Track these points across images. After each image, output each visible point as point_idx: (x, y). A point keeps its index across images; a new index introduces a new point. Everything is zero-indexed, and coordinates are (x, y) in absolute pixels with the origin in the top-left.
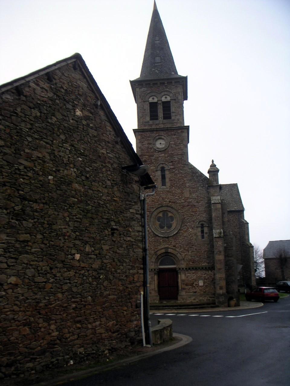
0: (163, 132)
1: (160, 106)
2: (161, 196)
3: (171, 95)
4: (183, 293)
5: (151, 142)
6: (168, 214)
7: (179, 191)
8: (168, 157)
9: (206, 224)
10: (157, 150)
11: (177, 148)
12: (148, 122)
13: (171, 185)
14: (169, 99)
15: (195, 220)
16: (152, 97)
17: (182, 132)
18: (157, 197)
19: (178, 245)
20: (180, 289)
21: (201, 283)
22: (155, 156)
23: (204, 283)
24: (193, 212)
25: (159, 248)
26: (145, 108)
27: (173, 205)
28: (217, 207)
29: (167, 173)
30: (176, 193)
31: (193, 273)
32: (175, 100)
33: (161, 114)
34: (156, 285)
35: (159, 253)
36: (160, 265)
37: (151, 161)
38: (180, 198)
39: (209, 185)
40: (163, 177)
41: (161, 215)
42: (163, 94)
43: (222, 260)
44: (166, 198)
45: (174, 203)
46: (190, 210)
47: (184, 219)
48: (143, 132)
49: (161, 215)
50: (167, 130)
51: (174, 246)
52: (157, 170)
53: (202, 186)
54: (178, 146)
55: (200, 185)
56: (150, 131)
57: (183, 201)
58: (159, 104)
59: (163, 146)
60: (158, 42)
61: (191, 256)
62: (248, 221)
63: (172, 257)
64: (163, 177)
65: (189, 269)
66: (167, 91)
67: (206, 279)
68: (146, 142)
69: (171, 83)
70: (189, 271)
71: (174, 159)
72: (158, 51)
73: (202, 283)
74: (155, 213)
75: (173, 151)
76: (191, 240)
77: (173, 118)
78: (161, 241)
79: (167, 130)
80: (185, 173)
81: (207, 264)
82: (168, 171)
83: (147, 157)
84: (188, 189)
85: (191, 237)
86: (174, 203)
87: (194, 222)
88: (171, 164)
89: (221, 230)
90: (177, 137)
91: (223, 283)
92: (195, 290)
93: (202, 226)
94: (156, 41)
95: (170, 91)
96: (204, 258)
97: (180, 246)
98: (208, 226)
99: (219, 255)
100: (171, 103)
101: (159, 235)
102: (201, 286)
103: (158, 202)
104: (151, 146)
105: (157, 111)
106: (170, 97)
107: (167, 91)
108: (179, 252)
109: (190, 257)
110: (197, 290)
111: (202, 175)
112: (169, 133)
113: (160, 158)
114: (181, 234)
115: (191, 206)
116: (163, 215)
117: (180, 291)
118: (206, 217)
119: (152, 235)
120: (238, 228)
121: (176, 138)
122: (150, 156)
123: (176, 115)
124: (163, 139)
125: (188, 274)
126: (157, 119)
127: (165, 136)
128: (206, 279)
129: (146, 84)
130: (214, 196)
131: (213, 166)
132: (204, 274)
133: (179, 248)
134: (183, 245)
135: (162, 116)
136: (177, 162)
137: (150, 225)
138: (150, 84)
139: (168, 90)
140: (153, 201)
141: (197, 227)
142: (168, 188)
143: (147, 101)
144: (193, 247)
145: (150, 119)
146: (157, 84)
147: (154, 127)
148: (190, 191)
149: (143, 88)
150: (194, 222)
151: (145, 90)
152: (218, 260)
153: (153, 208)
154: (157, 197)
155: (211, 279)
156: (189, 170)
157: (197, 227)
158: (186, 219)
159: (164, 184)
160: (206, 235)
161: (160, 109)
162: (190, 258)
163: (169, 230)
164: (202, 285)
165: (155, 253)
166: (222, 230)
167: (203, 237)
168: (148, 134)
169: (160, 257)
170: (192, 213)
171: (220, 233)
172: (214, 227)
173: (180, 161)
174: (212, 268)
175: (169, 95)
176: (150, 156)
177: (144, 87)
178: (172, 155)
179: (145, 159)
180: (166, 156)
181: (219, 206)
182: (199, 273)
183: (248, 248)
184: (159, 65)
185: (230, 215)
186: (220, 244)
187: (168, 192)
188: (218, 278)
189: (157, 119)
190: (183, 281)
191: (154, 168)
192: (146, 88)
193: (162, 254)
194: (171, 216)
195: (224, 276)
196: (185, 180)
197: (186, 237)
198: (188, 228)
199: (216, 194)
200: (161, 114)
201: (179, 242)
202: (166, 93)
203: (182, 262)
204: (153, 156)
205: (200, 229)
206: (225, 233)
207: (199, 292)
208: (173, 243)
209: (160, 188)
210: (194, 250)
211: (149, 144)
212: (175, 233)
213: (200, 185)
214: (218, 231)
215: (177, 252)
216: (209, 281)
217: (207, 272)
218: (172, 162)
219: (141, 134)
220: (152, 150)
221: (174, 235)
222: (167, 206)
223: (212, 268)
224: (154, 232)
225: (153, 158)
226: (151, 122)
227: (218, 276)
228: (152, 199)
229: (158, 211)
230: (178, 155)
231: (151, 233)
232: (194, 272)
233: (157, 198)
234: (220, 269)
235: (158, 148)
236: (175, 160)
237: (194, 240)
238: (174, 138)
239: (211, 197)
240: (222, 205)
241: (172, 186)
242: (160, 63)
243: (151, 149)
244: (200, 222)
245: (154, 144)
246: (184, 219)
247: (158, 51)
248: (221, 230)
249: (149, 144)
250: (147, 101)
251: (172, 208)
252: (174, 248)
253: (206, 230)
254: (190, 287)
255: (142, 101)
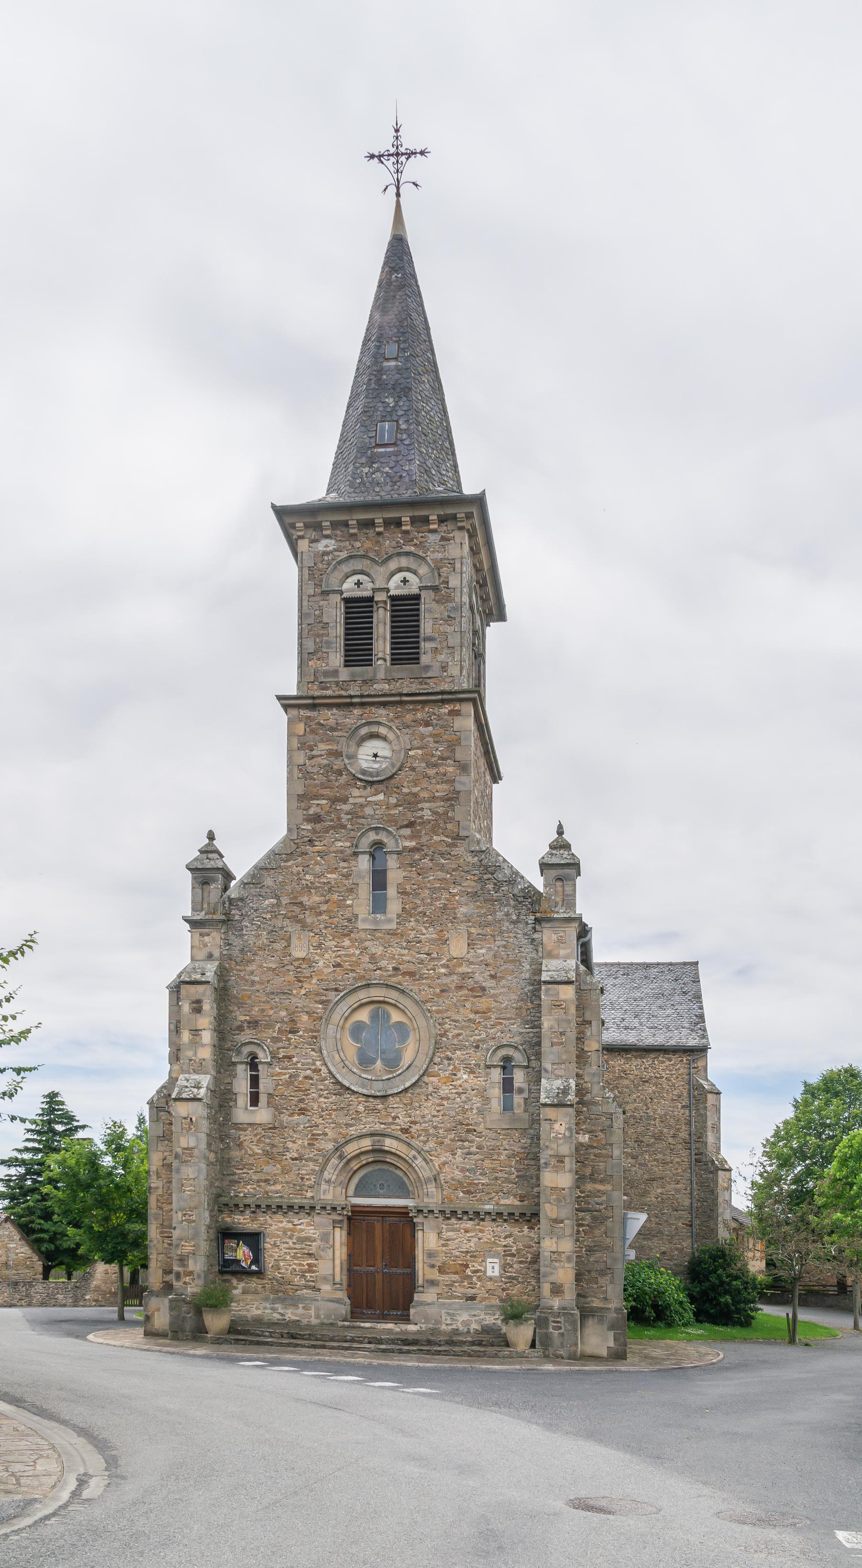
0: (382, 711)
1: (381, 611)
2: (366, 948)
3: (423, 570)
4: (426, 1296)
5: (342, 747)
6: (389, 1017)
7: (430, 934)
8: (397, 806)
9: (518, 1058)
10: (361, 780)
11: (431, 772)
12: (335, 673)
13: (404, 909)
14: (414, 585)
15: (483, 1041)
16: (355, 578)
17: (454, 713)
18: (352, 951)
19: (417, 1127)
20: (420, 1282)
21: (493, 1268)
22: (351, 800)
23: (504, 1267)
24: (476, 1012)
25: (353, 1131)
26: (325, 620)
27: (406, 983)
28: (562, 996)
29: (392, 862)
30: (420, 942)
31: (467, 1231)
32: (435, 589)
33: (382, 646)
34: (338, 1262)
35: (351, 1149)
36: (356, 1195)
37: (339, 819)
38: (433, 959)
39: (538, 915)
40: (379, 881)
41: (364, 1016)
42: (393, 565)
43: (564, 1189)
44: (382, 957)
45: (411, 974)
46: (468, 1005)
47: (442, 1036)
48: (313, 707)
49: (364, 1016)
50: (401, 703)
51: (405, 1131)
52: (356, 854)
53: (514, 917)
54: (435, 765)
55: (507, 914)
56: (338, 706)
57: (443, 970)
58: (377, 602)
59: (384, 766)
60: (393, 363)
61: (463, 1170)
62: (216, 837)
63: (397, 1167)
64: (379, 881)
65: (453, 1213)
66: (407, 554)
67: (513, 1255)
68: (323, 747)
69: (426, 520)
70: (453, 1221)
71: (420, 813)
72: (391, 401)
73: (497, 1267)
74: (343, 1008)
75: (416, 785)
76: (464, 1111)
77: (425, 659)
78: (361, 1108)
79: (401, 703)
80: (454, 870)
81: (517, 1203)
82: (395, 856)
83: (324, 802)
84: (463, 927)
85: (465, 1102)
86: (411, 974)
87: (477, 1047)
88: (407, 832)
89: (571, 1081)
90: (435, 732)
91: (565, 1274)
92: (471, 1292)
93: (507, 1065)
94: (388, 360)
95: (421, 554)
96: (507, 1180)
97: (426, 1130)
98: (527, 1067)
99: (557, 1170)
100: (422, 597)
101: (353, 1088)
102: (491, 1279)
103: (353, 970)
104: (338, 764)
105: (369, 632)
106: (420, 579)
107: (407, 554)
108: (419, 1153)
109: (457, 1172)
110: (479, 1289)
111: (515, 877)
112: (409, 717)
113: (368, 811)
114: (431, 1089)
115: (472, 990)
116: (374, 1017)
117: (421, 1289)
118: (521, 1033)
119: (331, 1087)
120: (683, 1107)
121: (430, 736)
122: (334, 800)
123: (435, 650)
124: (384, 739)
125: (450, 1234)
126: (369, 662)
127: (390, 728)
128: (513, 1255)
129: (334, 525)
130: (557, 957)
131: (560, 845)
132: (505, 1238)
133: (422, 1138)
134: (435, 1128)
135: (388, 651)
136: (429, 826)
137: (325, 1052)
138: (346, 524)
139: (413, 549)
140: (338, 965)
141: (488, 1067)
142: (389, 921)
143: (334, 592)
144: (471, 1137)
145: (346, 661)
146: (370, 524)
147: (354, 691)
148: (469, 934)
149: (324, 542)
150: (477, 1047)
151: (331, 548)
152: (552, 1189)
153: (336, 990)
154: (352, 951)
155: (529, 1256)
156: (470, 859)
157: (488, 1067)
158: (450, 1035)
159: (379, 905)
160: (518, 1099)
161: (381, 626)
162: (458, 1175)
163: (391, 1072)
164: (497, 1273)
165: (337, 1149)
166: (573, 1083)
167: (508, 1107)
168: (329, 716)
169: (355, 1165)
170: (472, 1016)
171: (565, 1091)
172: (546, 1071)
173: (441, 822)
174: (531, 1217)
175: (415, 572)
176: (334, 800)
177: (327, 537)
178: (412, 802)
179: (318, 810)
180: (393, 800)
181: (568, 993)
182: (489, 1230)
183: (711, 1172)
184: (389, 455)
185: (663, 1062)
186: (562, 1130)
187: (392, 933)
188: (546, 1254)
189: (369, 662)
190: (431, 1254)
191: (348, 844)
192: (333, 542)
193: (363, 1158)
194: (399, 1023)
195: (567, 1246)
196: (454, 895)
197: (448, 1099)
198: (455, 1067)
199: (562, 952)
200: (382, 646)
201: (423, 1117)
202: (404, 562)
203: (431, 1188)
204: (345, 800)
205: (496, 1075)
206: (588, 1097)
207: (484, 1299)
208: (403, 1121)
209: (365, 920)
210: (474, 1149)
211: (337, 754)
212: (408, 1084)
213: (507, 914)
214: (558, 1083)
215: (413, 1153)
216: (521, 1262)
217: (516, 1231)
218: (410, 825)
219: (308, 718)
220: (343, 779)
221: (406, 1090)
222: (388, 986)
223: (531, 1217)
224: (338, 1076)
225: (346, 807)
226: (344, 674)
227: (548, 1245)
228: (336, 957)
229: (353, 1000)
230: (433, 799)
231: (325, 1079)
232: (469, 1225)
233: (353, 955)
234: (556, 1221)
235: (364, 772)
236: (421, 817)
237: (475, 1111)
238: (423, 737)
239: (544, 962)
240: (579, 991)
241: (406, 914)
242: (395, 444)
243: (341, 775)
244: (498, 1048)
245: (353, 757)
246: (442, 1036)
247: (391, 401)
248: (571, 1081)
249: (337, 754)
250: (334, 592)
251: (403, 992)
252: (404, 1137)
253: (519, 1078)
254: (456, 1277)
255: (318, 591)
